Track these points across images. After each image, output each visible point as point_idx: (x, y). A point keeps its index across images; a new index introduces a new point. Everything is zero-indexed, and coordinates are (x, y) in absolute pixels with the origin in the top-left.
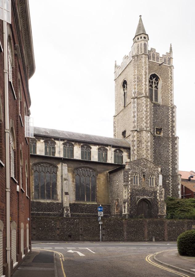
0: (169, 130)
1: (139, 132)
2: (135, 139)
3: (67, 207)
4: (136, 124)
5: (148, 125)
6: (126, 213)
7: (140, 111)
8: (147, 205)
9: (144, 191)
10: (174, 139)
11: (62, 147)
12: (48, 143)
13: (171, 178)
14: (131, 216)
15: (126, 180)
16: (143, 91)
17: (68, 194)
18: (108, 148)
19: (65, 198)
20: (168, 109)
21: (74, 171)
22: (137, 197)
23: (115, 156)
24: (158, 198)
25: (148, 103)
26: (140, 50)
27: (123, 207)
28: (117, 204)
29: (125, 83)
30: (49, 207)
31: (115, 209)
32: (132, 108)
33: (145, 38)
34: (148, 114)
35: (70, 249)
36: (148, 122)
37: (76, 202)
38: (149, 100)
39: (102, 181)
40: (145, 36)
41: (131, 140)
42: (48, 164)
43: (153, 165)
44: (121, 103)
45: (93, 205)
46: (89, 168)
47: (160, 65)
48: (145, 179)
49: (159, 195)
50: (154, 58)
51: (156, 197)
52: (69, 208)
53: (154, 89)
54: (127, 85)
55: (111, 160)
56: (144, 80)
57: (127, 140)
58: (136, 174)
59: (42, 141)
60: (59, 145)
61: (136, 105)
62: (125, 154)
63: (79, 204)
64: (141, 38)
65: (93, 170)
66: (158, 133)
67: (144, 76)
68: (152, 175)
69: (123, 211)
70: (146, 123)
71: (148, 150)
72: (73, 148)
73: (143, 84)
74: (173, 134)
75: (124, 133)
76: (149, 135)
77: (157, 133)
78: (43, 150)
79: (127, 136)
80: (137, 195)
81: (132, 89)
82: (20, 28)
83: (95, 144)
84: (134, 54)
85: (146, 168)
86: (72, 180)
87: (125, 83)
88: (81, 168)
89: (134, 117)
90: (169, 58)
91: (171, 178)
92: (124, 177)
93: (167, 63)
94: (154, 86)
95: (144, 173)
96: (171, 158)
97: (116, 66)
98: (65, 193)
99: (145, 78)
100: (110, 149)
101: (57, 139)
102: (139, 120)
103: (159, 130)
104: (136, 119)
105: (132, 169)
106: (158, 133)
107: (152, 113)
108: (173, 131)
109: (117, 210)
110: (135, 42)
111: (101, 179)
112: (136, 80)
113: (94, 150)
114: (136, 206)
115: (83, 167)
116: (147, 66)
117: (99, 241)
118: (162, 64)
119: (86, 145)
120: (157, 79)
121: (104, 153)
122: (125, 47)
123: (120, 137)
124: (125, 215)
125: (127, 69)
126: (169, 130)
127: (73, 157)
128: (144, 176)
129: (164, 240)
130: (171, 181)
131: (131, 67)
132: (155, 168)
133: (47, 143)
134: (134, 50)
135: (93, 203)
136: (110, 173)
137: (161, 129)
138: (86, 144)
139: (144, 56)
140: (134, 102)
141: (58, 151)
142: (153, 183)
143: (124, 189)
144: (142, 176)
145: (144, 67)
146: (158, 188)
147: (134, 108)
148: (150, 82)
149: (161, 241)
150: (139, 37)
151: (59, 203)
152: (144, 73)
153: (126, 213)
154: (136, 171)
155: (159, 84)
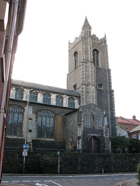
0: (107, 86)
1: (88, 85)
2: (84, 90)
3: (30, 142)
4: (84, 80)
5: (93, 81)
6: (80, 148)
7: (87, 71)
8: (96, 141)
9: (93, 130)
10: (112, 92)
11: (29, 94)
12: (18, 90)
13: (110, 120)
14: (84, 151)
15: (79, 120)
16: (89, 59)
17: (32, 132)
18: (64, 96)
19: (29, 135)
20: (106, 72)
21: (36, 113)
22: (89, 134)
23: (69, 103)
24: (104, 135)
25: (93, 66)
26: (86, 34)
27: (77, 144)
28: (71, 140)
29: (76, 53)
30: (14, 142)
31: (69, 145)
32: (81, 71)
33: (89, 28)
34: (93, 73)
35: (37, 182)
36: (93, 78)
37: (37, 139)
38: (93, 64)
39: (59, 121)
40: (89, 27)
41: (81, 91)
42: (18, 106)
43: (100, 109)
44: (73, 66)
45: (51, 141)
46: (48, 110)
47: (99, 44)
48: (95, 120)
49: (105, 133)
50: (95, 40)
51: (102, 134)
52: (31, 144)
53: (96, 58)
54: (77, 54)
55: (65, 104)
56: (89, 51)
57: (77, 91)
58: (87, 116)
59: (14, 88)
60: (26, 92)
61: (84, 67)
62: (76, 101)
63: (40, 140)
64: (87, 28)
65: (53, 112)
66: (100, 87)
67: (89, 49)
68: (100, 116)
69: (78, 146)
70: (92, 79)
71: (94, 99)
72: (37, 95)
73: (89, 54)
74: (110, 88)
75: (75, 86)
76: (94, 88)
77: (99, 87)
78: (14, 95)
79: (77, 88)
80: (88, 133)
81: (81, 57)
82: (13, 10)
83: (54, 93)
84: (83, 36)
85: (95, 111)
86: (35, 120)
87: (76, 53)
88: (43, 110)
89: (83, 75)
90: (104, 41)
91: (110, 120)
92: (78, 118)
93: (104, 43)
94: (95, 56)
95: (93, 115)
96: (110, 105)
97: (69, 43)
98: (29, 130)
99: (90, 51)
100: (65, 97)
101: (26, 88)
102: (87, 77)
103: (100, 85)
104: (84, 76)
105: (84, 112)
106: (100, 87)
107: (95, 73)
108: (110, 86)
109: (71, 146)
110: (83, 29)
111: (59, 119)
112: (84, 51)
113: (53, 96)
114: (88, 142)
115: (45, 110)
116: (91, 44)
117: (57, 173)
118: (100, 43)
119: (47, 93)
120: (98, 52)
121: (60, 100)
122: (77, 32)
123: (73, 89)
124: (80, 149)
125: (78, 45)
126: (107, 86)
127: (37, 101)
128: (93, 117)
129: (56, 173)
130: (111, 123)
131: (81, 44)
132: (101, 112)
133: (17, 91)
134: (83, 34)
135: (51, 140)
136: (66, 115)
137: (102, 84)
138: (47, 92)
139: (89, 37)
140: (83, 65)
141: (25, 97)
142: (100, 124)
143: (78, 128)
144: (92, 118)
145: (90, 44)
146: (104, 127)
147: (83, 68)
148: (93, 53)
149: (109, 172)
150: (86, 27)
151: (23, 139)
152: (90, 48)
153: (80, 148)
154: (88, 114)
155: (99, 55)
